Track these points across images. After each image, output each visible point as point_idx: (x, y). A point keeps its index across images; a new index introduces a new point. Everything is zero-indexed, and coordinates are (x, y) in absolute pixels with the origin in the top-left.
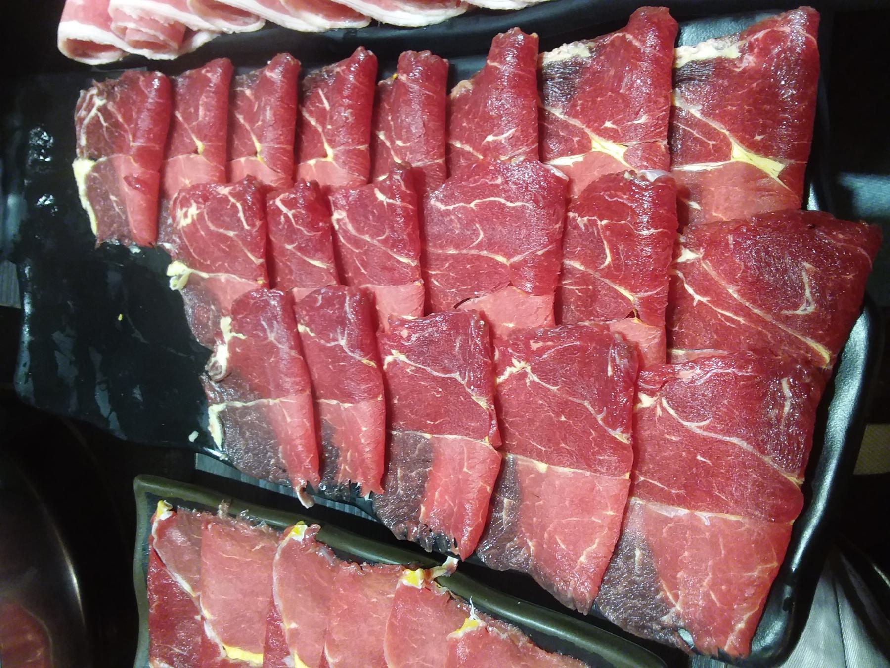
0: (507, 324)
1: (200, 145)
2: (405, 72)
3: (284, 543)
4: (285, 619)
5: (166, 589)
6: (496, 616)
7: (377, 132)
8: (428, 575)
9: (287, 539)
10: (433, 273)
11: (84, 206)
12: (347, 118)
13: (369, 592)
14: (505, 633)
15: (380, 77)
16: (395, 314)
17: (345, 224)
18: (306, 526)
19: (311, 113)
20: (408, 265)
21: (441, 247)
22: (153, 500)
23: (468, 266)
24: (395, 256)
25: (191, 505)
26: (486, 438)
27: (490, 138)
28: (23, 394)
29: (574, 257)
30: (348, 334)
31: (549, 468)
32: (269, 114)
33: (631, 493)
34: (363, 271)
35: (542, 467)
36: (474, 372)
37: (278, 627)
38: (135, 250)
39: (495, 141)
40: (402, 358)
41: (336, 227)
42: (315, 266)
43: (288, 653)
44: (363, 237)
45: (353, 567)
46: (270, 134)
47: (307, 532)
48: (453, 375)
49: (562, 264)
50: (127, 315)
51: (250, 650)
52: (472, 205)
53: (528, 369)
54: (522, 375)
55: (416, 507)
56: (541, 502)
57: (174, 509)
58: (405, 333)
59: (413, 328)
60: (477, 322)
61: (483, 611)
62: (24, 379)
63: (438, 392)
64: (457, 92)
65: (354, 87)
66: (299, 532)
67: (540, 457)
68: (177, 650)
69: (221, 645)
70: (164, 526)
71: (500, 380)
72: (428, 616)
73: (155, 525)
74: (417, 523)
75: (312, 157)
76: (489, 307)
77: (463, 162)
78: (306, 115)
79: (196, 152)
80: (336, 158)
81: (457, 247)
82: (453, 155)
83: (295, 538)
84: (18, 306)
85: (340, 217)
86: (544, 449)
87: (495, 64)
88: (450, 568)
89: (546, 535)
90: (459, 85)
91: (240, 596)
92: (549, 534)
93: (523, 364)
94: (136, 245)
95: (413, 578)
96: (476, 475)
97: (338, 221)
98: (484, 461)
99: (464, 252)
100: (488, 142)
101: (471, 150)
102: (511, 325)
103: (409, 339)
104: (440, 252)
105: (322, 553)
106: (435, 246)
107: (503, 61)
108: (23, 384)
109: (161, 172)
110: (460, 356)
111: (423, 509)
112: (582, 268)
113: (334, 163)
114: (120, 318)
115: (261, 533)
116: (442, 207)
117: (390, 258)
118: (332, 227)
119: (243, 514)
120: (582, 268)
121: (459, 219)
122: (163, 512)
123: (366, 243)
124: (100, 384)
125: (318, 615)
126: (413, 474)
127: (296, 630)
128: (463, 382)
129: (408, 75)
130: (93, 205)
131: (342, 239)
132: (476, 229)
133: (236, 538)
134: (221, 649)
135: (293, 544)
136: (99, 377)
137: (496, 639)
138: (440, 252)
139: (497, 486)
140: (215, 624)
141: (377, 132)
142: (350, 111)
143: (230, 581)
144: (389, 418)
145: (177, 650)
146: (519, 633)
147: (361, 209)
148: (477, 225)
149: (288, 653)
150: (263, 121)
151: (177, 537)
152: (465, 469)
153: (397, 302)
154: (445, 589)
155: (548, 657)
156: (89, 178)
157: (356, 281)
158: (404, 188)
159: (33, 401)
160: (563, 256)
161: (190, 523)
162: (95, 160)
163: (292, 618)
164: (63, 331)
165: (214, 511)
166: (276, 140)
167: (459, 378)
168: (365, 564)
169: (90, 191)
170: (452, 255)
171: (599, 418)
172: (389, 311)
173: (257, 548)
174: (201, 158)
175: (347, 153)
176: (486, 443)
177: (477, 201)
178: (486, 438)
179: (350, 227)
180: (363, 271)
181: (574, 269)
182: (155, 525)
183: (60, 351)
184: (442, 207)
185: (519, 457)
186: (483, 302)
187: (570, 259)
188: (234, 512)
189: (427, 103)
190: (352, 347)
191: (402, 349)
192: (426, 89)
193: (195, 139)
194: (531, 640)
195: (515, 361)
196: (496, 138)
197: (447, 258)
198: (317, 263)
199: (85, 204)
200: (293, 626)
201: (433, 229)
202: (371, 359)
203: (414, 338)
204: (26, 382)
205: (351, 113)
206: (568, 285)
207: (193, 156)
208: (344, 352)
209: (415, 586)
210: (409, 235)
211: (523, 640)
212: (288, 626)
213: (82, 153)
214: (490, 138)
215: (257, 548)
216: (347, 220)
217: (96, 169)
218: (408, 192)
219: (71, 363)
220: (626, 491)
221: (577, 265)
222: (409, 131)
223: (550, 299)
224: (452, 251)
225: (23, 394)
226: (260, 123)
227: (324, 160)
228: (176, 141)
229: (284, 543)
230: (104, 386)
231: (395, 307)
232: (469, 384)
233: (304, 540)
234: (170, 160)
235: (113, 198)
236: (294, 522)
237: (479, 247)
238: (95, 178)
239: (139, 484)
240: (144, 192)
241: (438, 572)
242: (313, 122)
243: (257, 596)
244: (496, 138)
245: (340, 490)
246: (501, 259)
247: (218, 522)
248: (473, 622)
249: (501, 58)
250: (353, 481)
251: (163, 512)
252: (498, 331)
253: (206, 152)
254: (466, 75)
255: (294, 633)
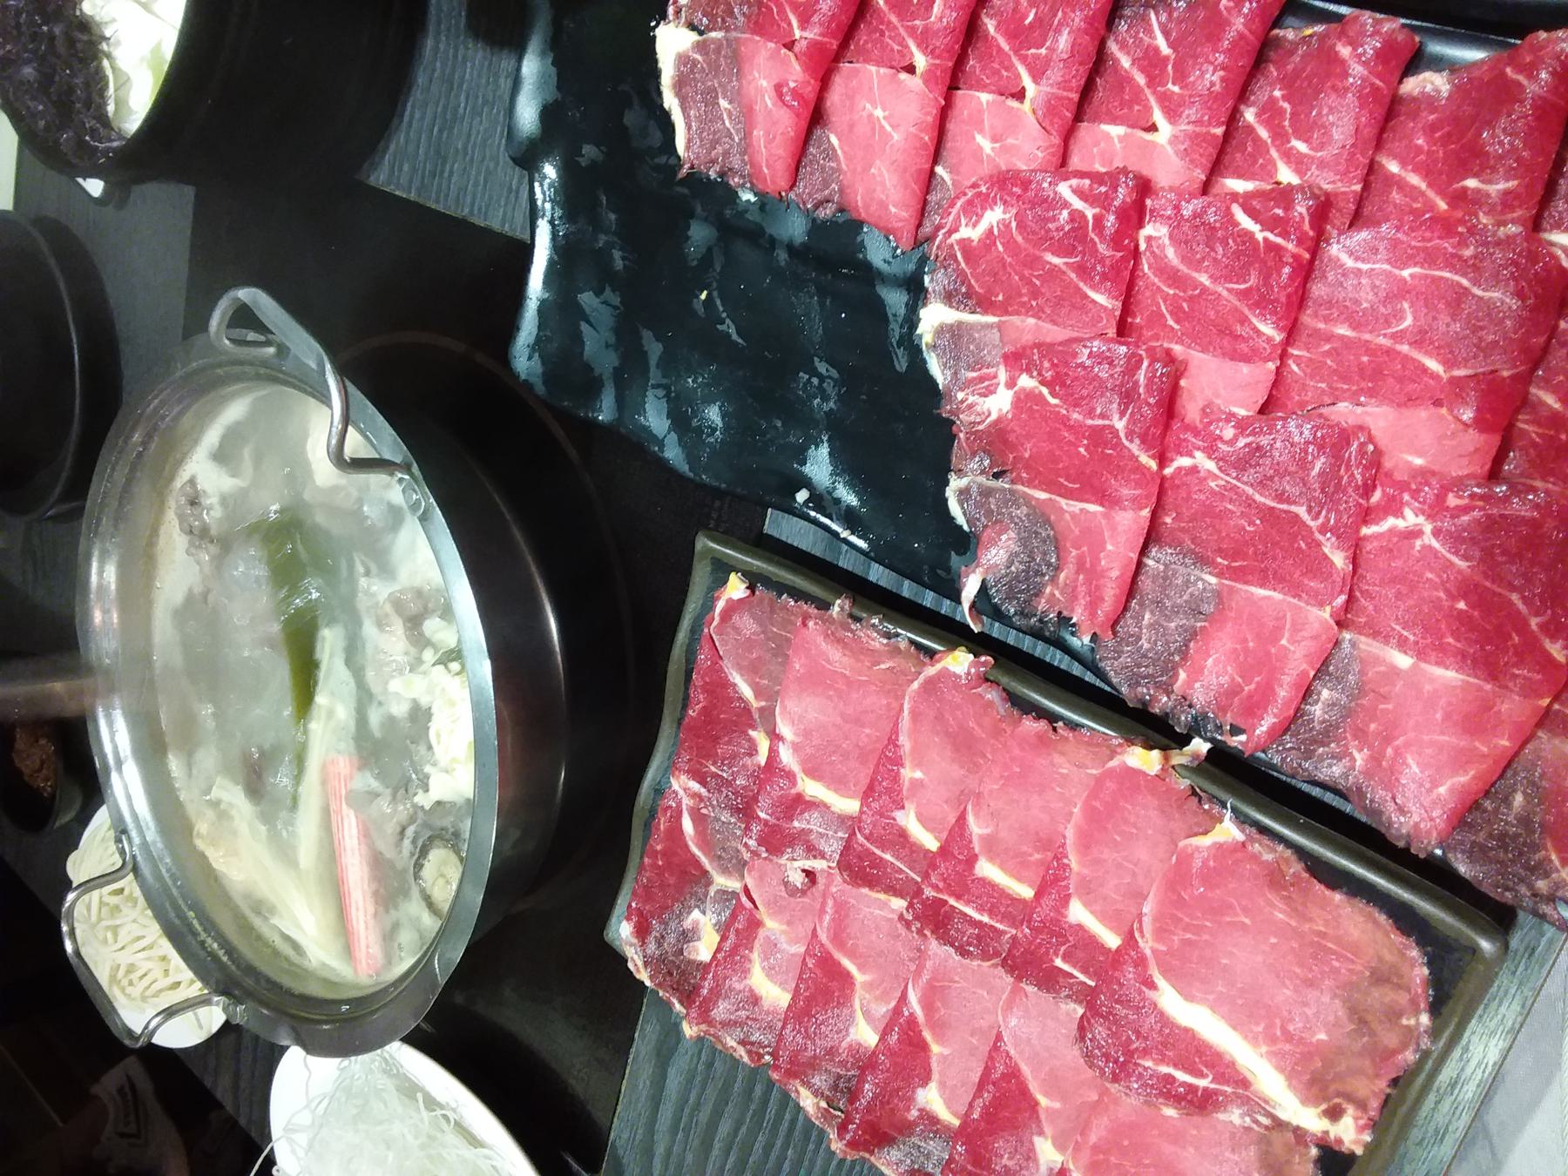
0: (1410, 458)
1: (921, 61)
2: (1350, 44)
3: (931, 671)
4: (907, 763)
5: (720, 687)
6: (1264, 830)
7: (1242, 107)
8: (1166, 759)
9: (939, 666)
10: (1296, 352)
11: (666, 106)
12: (1212, 84)
13: (1058, 759)
14: (1268, 853)
15: (1277, 23)
16: (1218, 401)
17: (1162, 247)
18: (971, 656)
19: (1123, 46)
20: (1269, 340)
21: (1327, 319)
22: (722, 570)
23: (1365, 359)
24: (1255, 321)
25: (781, 588)
26: (1328, 609)
27: (1472, 183)
28: (523, 377)
29: (1547, 384)
30: (1132, 414)
31: (1414, 666)
32: (1064, 41)
33: (1540, 724)
34: (1171, 322)
35: (1404, 661)
36: (1338, 512)
37: (898, 773)
38: (747, 196)
39: (1478, 191)
40: (1211, 465)
41: (1143, 246)
42: (1093, 301)
43: (903, 807)
44: (1195, 275)
45: (1042, 725)
46: (1055, 74)
47: (973, 664)
48: (1293, 508)
49: (1527, 393)
50: (715, 294)
51: (836, 791)
52: (1406, 273)
53: (1428, 528)
54: (1415, 533)
55: (1171, 670)
56: (1390, 706)
57: (752, 588)
58: (1229, 433)
59: (1242, 426)
60: (1362, 445)
61: (1241, 819)
62: (526, 352)
63: (1251, 523)
64: (1411, 85)
65: (1241, 36)
66: (960, 662)
67: (1403, 645)
68: (713, 769)
69: (800, 776)
70: (733, 607)
71: (1365, 531)
72: (1146, 814)
73: (720, 605)
74: (1168, 693)
75: (1114, 120)
76: (1382, 424)
77: (1396, 196)
78: (1113, 47)
79: (911, 69)
80: (1174, 140)
81: (1355, 326)
82: (1376, 185)
83: (952, 669)
84: (526, 237)
85: (1154, 234)
86: (1412, 638)
87: (1521, 78)
88: (1195, 756)
89: (1389, 751)
90: (1421, 76)
91: (839, 720)
92: (1397, 751)
93: (1421, 519)
94: (751, 189)
95: (1144, 760)
96: (1299, 655)
97: (1149, 239)
98: (1314, 638)
99: (1367, 337)
100: (1465, 189)
101: (1423, 186)
102: (1418, 461)
103: (1231, 442)
104: (1321, 326)
105: (992, 695)
106: (1316, 315)
107: (1532, 77)
108: (524, 358)
109: (824, 83)
110: (1316, 486)
111: (1182, 675)
112: (1557, 406)
113: (1169, 148)
114: (703, 296)
115: (896, 651)
116: (1350, 263)
117: (1244, 320)
118: (1137, 246)
119: (875, 621)
120: (1557, 406)
121: (1374, 287)
122: (736, 588)
123: (1196, 285)
124: (654, 387)
125: (957, 771)
126: (1173, 625)
127: (921, 781)
128: (1312, 524)
129: (1355, 49)
130: (684, 109)
131: (1146, 267)
132: (1402, 311)
133: (857, 650)
134: (799, 781)
135: (946, 674)
136: (655, 375)
137: (1255, 858)
138: (1321, 326)
139: (1322, 671)
140: (796, 748)
141: (1242, 107)
142: (1222, 73)
143: (829, 698)
144: (1152, 536)
145: (713, 769)
146: (1294, 858)
147: (1202, 236)
148: (1406, 305)
149: (903, 807)
150: (1052, 50)
151: (747, 624)
152: (1284, 642)
153: (1221, 385)
154: (1188, 782)
155: (1328, 892)
156: (683, 60)
157: (1148, 334)
158: (1306, 226)
159: (540, 389)
160: (1530, 383)
161: (772, 611)
162: (701, 33)
163: (918, 765)
164: (598, 293)
165: (825, 606)
166: (1063, 85)
167: (1305, 517)
168: (1060, 724)
169: (680, 85)
170: (1342, 337)
171: (1534, 622)
172: (1208, 393)
173: (883, 666)
174: (914, 83)
175: (1195, 138)
176: (1326, 614)
177: (1417, 270)
178: (1328, 609)
179: (1170, 253)
180: (1171, 322)
181: (1542, 403)
182: (720, 605)
183: (588, 322)
184: (1350, 263)
185: (1363, 638)
186: (1377, 417)
187: (1540, 388)
188: (856, 612)
189: (1368, 96)
190: (1130, 434)
191: (1210, 451)
192: (1378, 76)
193: (914, 48)
194: (1309, 869)
195: (1408, 512)
196: (1481, 186)
197: (1329, 338)
198: (1100, 298)
199: (670, 101)
200: (918, 775)
201: (1318, 290)
202: (1153, 457)
203: (1241, 442)
204: (530, 358)
205: (1223, 79)
206: (1523, 424)
207: (903, 76)
208: (1118, 437)
209: (1145, 768)
210: (1289, 296)
211: (1296, 867)
212: (909, 773)
213: (678, 13)
214: (1472, 183)
215: (883, 666)
216: (1167, 241)
217: (701, 47)
218: (1311, 233)
219: (607, 346)
220: (1535, 720)
221: (1551, 400)
222: (1327, 134)
223: (1495, 440)
224: (1343, 330)
225: (523, 377)
226: (1043, 51)
227: (1148, 136)
228: (863, 36)
229: (931, 671)
230: (661, 393)
231: (1222, 392)
232: (1323, 530)
233: (968, 674)
234: (845, 66)
235: (724, 103)
236: (952, 647)
237: (1398, 337)
238: (695, 63)
239: (704, 543)
240: (798, 115)
241: (1178, 758)
242: (1126, 62)
243: (863, 726)
244: (1481, 186)
245: (1041, 621)
246: (1433, 365)
247: (831, 620)
248: (1228, 831)
249: (1530, 71)
250: (1065, 613)
251: (736, 588)
252: (1388, 464)
253: (929, 77)
254: (1438, 64)
255: (916, 785)
